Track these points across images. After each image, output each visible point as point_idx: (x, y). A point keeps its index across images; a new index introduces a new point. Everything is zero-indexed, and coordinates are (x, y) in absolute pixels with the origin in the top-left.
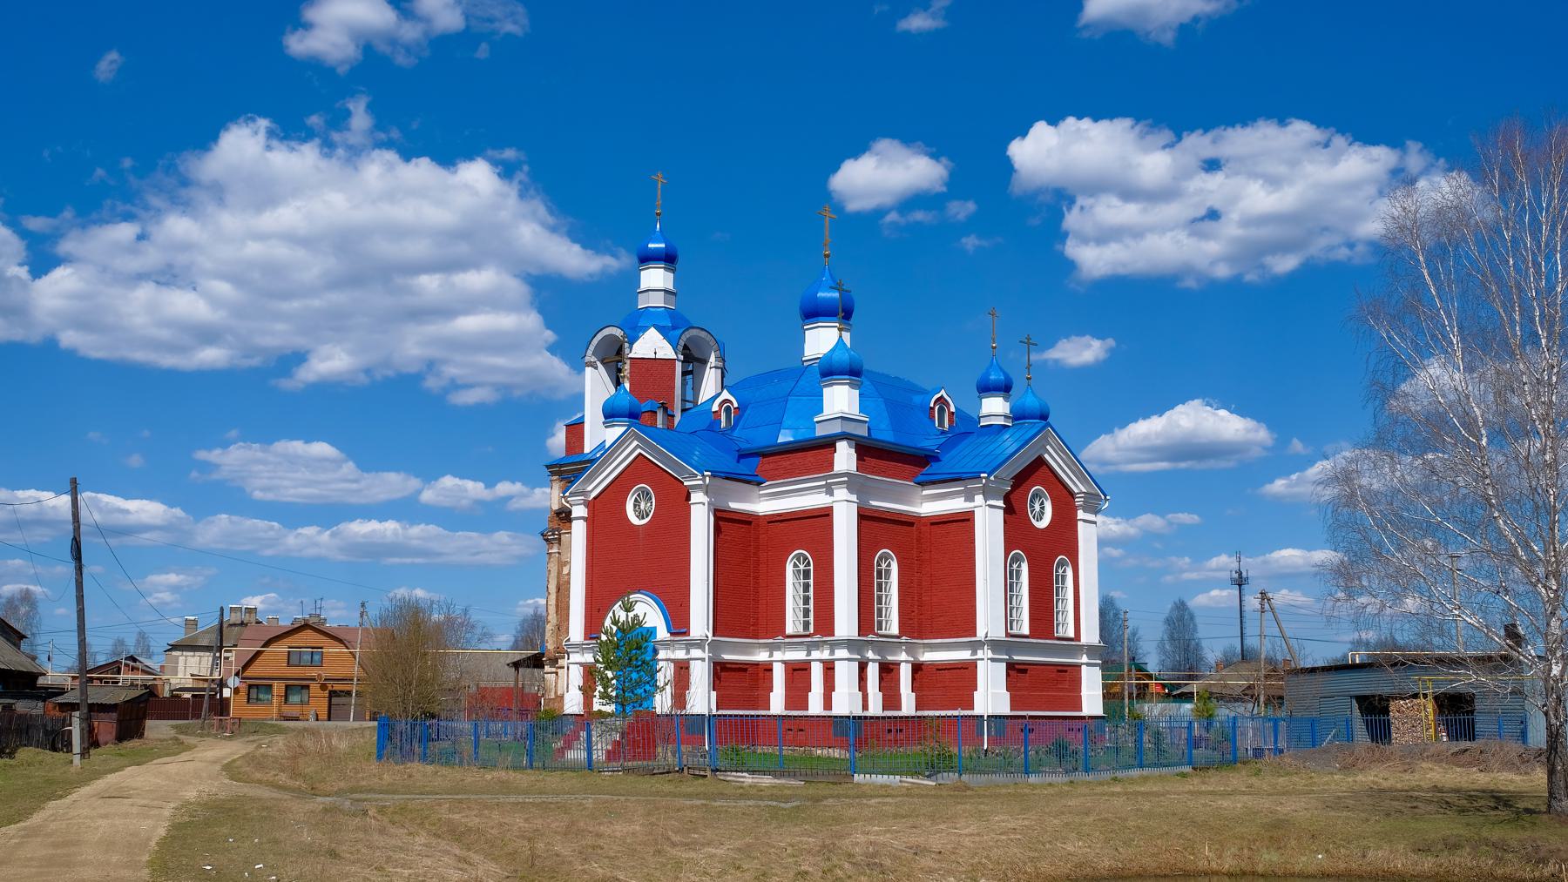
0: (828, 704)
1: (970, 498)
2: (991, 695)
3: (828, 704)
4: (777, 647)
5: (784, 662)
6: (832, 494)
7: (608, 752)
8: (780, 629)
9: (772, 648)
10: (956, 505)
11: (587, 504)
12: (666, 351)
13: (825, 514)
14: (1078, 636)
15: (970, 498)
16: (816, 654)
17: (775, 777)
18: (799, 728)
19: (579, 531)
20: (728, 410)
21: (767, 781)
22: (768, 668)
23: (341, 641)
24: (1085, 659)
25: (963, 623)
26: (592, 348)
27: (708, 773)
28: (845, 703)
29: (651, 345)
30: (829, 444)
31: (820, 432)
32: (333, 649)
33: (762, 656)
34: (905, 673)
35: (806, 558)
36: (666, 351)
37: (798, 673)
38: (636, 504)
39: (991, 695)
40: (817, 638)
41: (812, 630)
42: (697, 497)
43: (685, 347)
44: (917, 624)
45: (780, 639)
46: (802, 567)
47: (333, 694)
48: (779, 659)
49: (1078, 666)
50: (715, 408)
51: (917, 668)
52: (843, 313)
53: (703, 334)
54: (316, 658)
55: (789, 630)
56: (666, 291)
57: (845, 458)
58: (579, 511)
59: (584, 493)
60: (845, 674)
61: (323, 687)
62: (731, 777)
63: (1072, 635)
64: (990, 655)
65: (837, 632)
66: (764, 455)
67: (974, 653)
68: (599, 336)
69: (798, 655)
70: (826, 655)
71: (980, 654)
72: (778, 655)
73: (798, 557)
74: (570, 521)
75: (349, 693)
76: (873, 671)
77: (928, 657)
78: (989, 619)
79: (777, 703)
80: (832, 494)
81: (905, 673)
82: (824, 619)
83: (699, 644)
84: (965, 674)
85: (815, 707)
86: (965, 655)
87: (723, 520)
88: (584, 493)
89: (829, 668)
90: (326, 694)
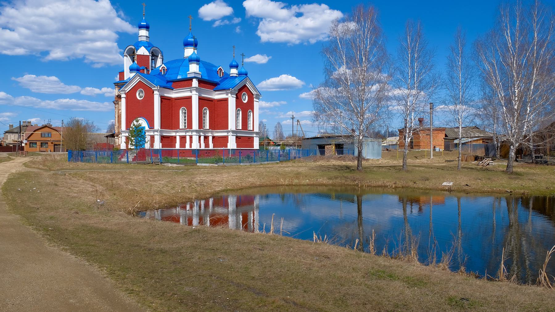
0: (191, 146)
1: (227, 95)
2: (232, 144)
3: (191, 146)
9: (176, 132)
10: (223, 96)
11: (125, 94)
12: (147, 53)
13: (190, 98)
15: (227, 95)
16: (187, 134)
18: (184, 153)
21: (175, 165)
22: (175, 137)
25: (224, 126)
29: (142, 51)
30: (191, 79)
32: (54, 132)
34: (210, 139)
36: (147, 53)
37: (183, 138)
39: (232, 144)
42: (156, 92)
44: (214, 126)
45: (178, 130)
47: (55, 145)
48: (178, 135)
49: (253, 137)
50: (160, 69)
52: (195, 45)
57: (195, 83)
58: (123, 96)
59: (124, 91)
60: (195, 139)
61: (52, 143)
62: (166, 164)
68: (128, 48)
69: (183, 134)
71: (229, 134)
72: (178, 134)
76: (202, 138)
77: (216, 134)
78: (232, 125)
79: (178, 146)
81: (210, 139)
83: (157, 131)
84: (226, 138)
85: (187, 147)
86: (225, 134)
87: (163, 99)
88: (124, 91)
89: (191, 137)
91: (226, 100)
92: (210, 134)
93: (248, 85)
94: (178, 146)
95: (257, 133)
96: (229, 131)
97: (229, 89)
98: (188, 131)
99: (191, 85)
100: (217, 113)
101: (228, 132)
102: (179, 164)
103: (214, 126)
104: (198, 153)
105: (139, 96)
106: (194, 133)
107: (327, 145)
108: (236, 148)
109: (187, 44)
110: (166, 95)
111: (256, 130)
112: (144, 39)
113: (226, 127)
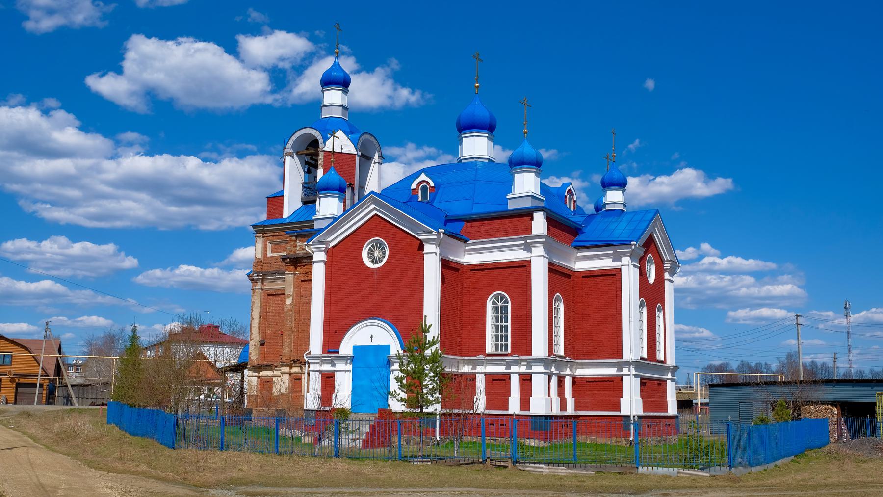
0: (525, 404)
1: (617, 258)
2: (631, 403)
3: (525, 404)
4: (481, 363)
5: (486, 374)
6: (529, 251)
7: (364, 441)
8: (481, 349)
9: (474, 364)
10: (606, 263)
11: (327, 252)
12: (350, 148)
13: (525, 266)
14: (665, 362)
15: (617, 258)
16: (514, 369)
17: (568, 467)
18: (500, 424)
19: (319, 273)
20: (424, 190)
21: (562, 471)
22: (473, 378)
23: (26, 349)
24: (669, 376)
25: (612, 348)
26: (291, 142)
27: (510, 465)
28: (543, 403)
29: (341, 143)
30: (528, 214)
31: (512, 206)
32: (18, 353)
33: (466, 369)
34: (568, 382)
35: (503, 297)
36: (350, 148)
37: (498, 385)
38: (371, 253)
39: (631, 403)
40: (515, 357)
41: (509, 351)
42: (428, 248)
43: (363, 144)
44: (578, 347)
45: (481, 357)
46: (500, 304)
47: (19, 385)
48: (483, 370)
49: (665, 381)
50: (414, 186)
51: (575, 380)
52: (489, 128)
53: (372, 139)
54: (7, 360)
55: (490, 348)
56: (343, 107)
57: (539, 224)
58: (320, 256)
59: (325, 242)
60: (538, 383)
61: (12, 380)
62: (529, 467)
63: (662, 359)
64: (633, 371)
65: (624, 357)
66: (468, 221)
67: (508, 368)
68: (297, 135)
69: (500, 369)
70: (523, 369)
71: (625, 371)
72: (480, 369)
73: (496, 297)
74: (311, 264)
75: (34, 385)
76: (554, 380)
77: (580, 372)
78: (633, 345)
79: (480, 404)
80: (529, 251)
81: (568, 382)
82: (522, 343)
83: (537, 361)
84: (614, 385)
85: (514, 406)
86: (612, 372)
87: (446, 265)
88: (325, 242)
89: (526, 380)
90: (14, 385)
91: (614, 275)
92: (568, 372)
93: (658, 238)
94: (480, 404)
95: (674, 370)
96: (628, 364)
97: (627, 244)
98: (517, 362)
99: (529, 230)
100: (591, 312)
101: (620, 366)
102: (575, 467)
103: (578, 347)
104: (545, 426)
105: (371, 258)
106: (539, 368)
107: (808, 403)
108: (641, 413)
109: (468, 126)
110: (452, 258)
111: (670, 362)
112: (338, 113)
113: (615, 350)
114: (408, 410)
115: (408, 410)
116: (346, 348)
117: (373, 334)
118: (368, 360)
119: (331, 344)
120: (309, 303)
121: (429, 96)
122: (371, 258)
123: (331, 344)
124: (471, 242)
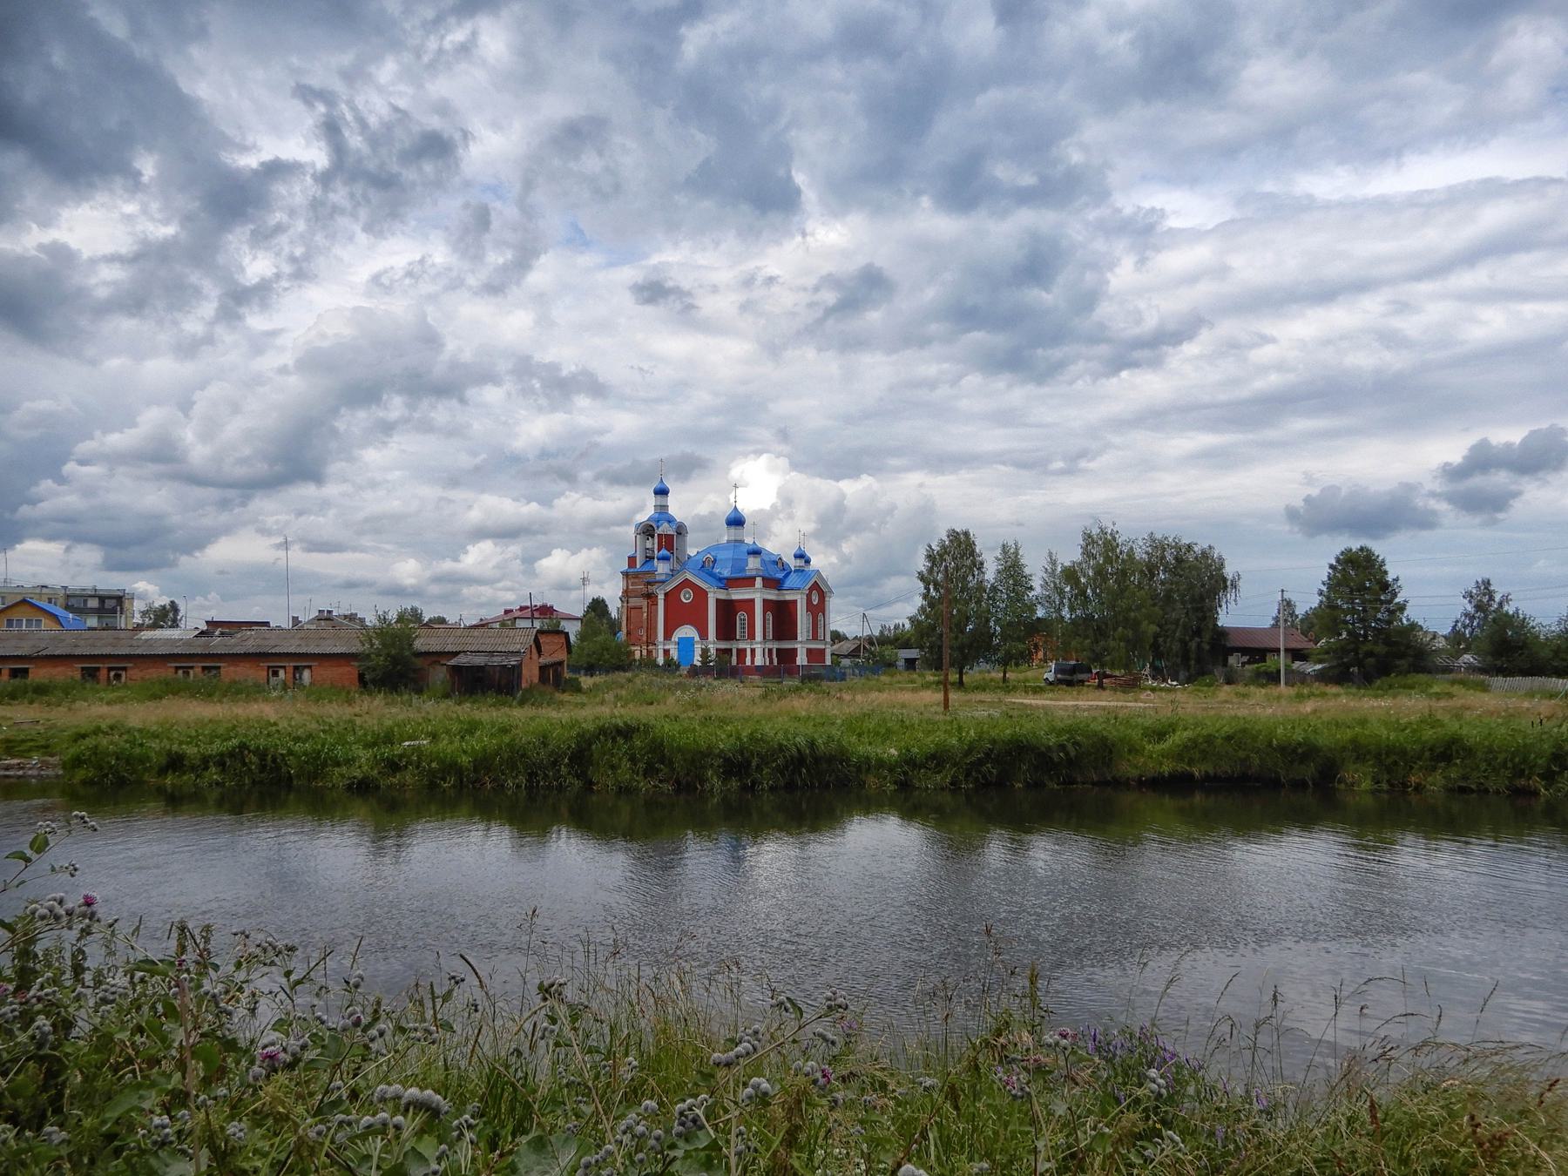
25: (793, 636)
28: (759, 661)
30: (754, 578)
37: (741, 653)
44: (778, 636)
57: (759, 581)
82: (752, 636)
85: (748, 662)
89: (753, 651)
105: (686, 597)
114: (655, 260)
115: (655, 260)
116: (675, 638)
117: (687, 631)
118: (686, 644)
119: (668, 636)
120: (656, 627)
121: (781, 172)
122: (686, 597)
123: (668, 636)
124: (770, 616)
